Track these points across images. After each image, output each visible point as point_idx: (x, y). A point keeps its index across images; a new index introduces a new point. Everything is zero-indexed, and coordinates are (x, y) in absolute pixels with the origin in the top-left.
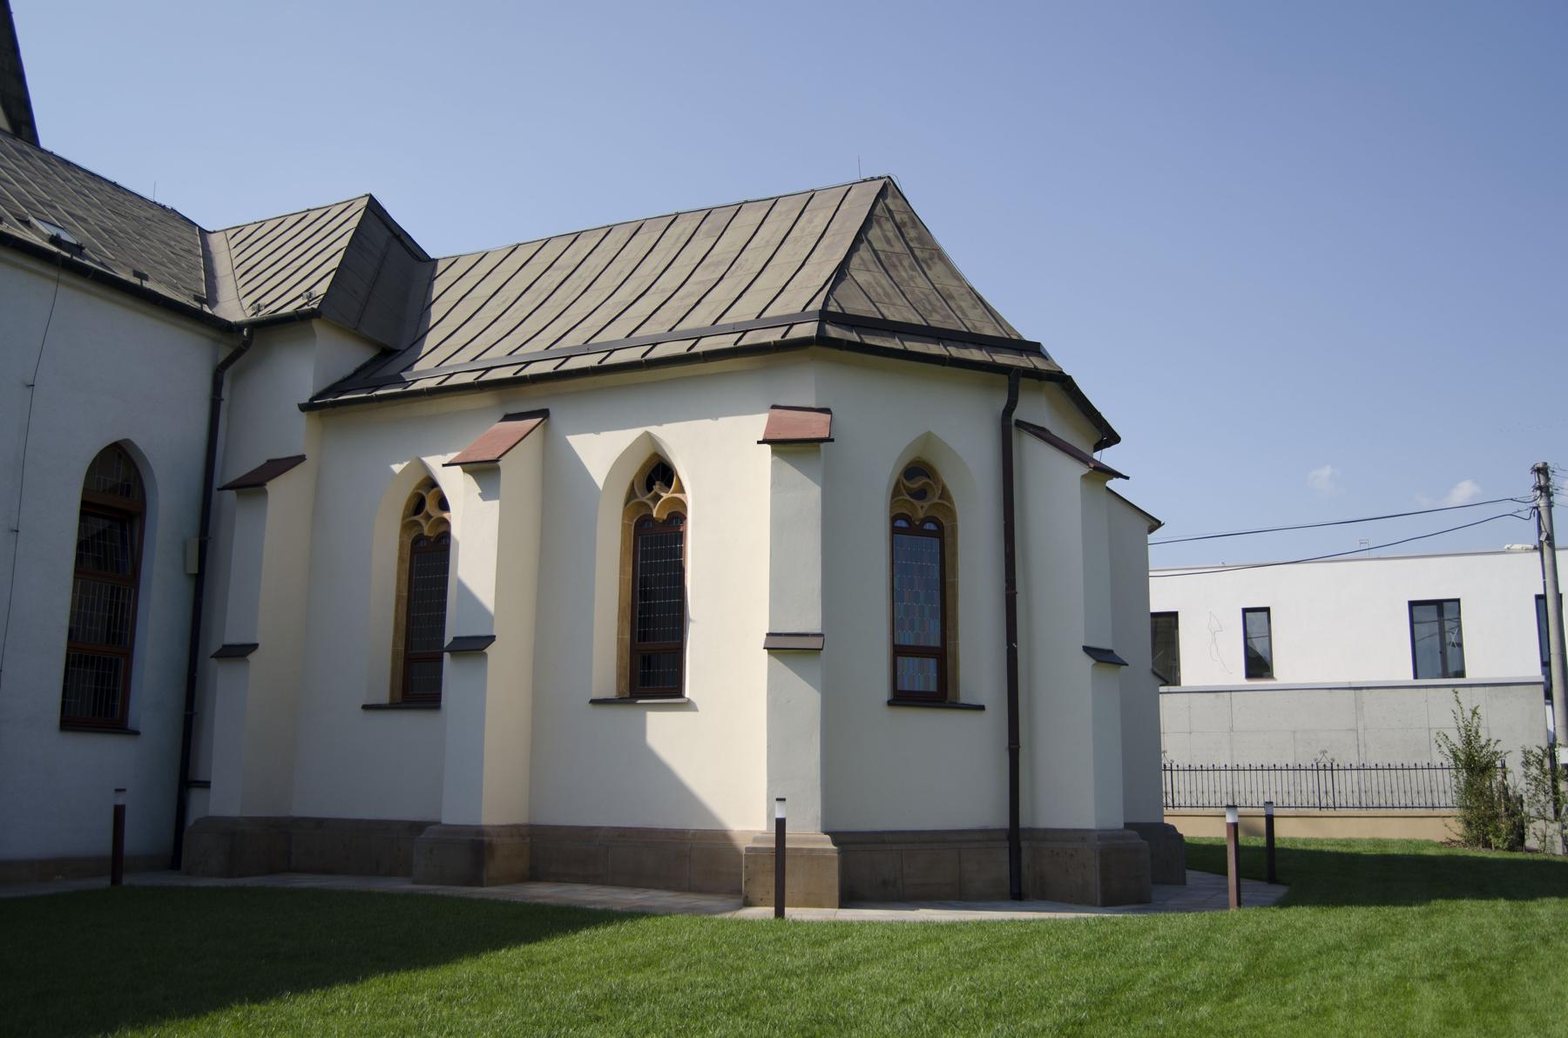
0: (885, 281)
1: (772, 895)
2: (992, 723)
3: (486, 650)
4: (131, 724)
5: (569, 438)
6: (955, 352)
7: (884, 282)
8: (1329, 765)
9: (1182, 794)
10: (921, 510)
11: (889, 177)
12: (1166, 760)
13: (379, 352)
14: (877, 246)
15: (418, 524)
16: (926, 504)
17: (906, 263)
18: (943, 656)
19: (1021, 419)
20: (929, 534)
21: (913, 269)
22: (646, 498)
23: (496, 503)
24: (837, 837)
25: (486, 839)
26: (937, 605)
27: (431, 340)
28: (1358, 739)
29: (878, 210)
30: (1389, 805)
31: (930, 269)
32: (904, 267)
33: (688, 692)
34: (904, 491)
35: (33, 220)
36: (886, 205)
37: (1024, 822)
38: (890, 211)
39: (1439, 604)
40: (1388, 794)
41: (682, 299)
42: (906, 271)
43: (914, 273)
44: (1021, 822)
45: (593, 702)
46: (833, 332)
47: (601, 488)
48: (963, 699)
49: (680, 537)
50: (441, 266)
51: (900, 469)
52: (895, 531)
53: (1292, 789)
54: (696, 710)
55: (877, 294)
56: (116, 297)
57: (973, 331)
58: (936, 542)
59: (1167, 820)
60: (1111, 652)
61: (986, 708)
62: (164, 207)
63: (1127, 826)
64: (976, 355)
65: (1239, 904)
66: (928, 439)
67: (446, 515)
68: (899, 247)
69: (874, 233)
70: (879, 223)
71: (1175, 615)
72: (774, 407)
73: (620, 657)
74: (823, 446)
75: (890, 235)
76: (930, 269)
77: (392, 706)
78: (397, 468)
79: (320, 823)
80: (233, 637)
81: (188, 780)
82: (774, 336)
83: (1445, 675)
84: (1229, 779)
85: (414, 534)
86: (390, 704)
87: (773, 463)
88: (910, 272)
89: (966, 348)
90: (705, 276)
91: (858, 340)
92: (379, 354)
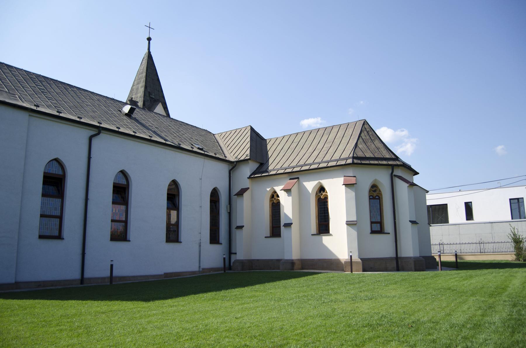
0: (365, 146)
1: (350, 270)
2: (391, 236)
3: (292, 226)
4: (220, 242)
5: (303, 183)
6: (380, 162)
7: (365, 147)
8: (442, 244)
9: (486, 249)
10: (375, 194)
11: (365, 120)
12: (13, 281)
13: (260, 164)
14: (363, 138)
15: (273, 200)
16: (376, 193)
17: (369, 141)
18: (381, 223)
19: (395, 174)
20: (377, 199)
21: (371, 142)
22: (320, 194)
23: (291, 197)
24: (361, 259)
25: (294, 262)
26: (379, 213)
27: (271, 161)
28: (492, 236)
29: (363, 129)
30: (502, 251)
31: (375, 142)
32: (369, 142)
33: (331, 232)
34: (371, 191)
35: (193, 144)
36: (365, 127)
37: (399, 256)
38: (365, 128)
39: (518, 199)
40: (465, 250)
41: (323, 151)
42: (370, 143)
43: (371, 143)
44: (398, 256)
45: (312, 235)
46: (356, 161)
47: (310, 192)
48: (386, 232)
49: (327, 202)
50: (268, 142)
51: (371, 186)
52: (370, 199)
53: (449, 249)
54: (333, 236)
55: (364, 150)
56: (213, 159)
57: (385, 157)
58: (378, 200)
59: (433, 255)
60: (415, 221)
61: (390, 233)
62: (204, 130)
63: (420, 256)
64: (385, 162)
65: (441, 270)
66: (376, 180)
67: (279, 198)
68: (368, 137)
69: (362, 135)
70: (363, 132)
71: (447, 204)
72: (344, 176)
73: (316, 226)
74: (355, 185)
75: (366, 134)
76: (375, 142)
77: (270, 237)
78: (268, 189)
79: (258, 260)
80: (239, 224)
81: (230, 253)
82: (343, 162)
83: (520, 218)
84: (468, 246)
85: (272, 202)
86: (270, 236)
87: (345, 188)
88: (370, 143)
89: (382, 161)
90: (327, 146)
91: (360, 162)
92: (260, 165)
